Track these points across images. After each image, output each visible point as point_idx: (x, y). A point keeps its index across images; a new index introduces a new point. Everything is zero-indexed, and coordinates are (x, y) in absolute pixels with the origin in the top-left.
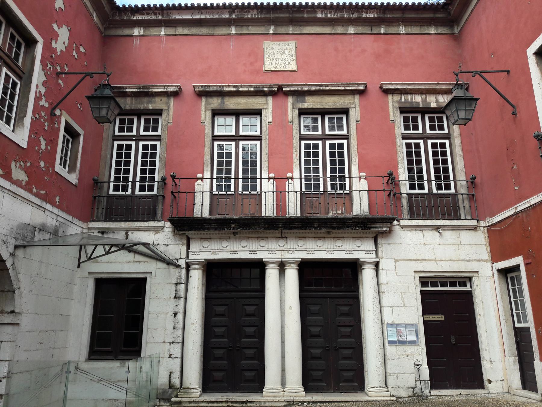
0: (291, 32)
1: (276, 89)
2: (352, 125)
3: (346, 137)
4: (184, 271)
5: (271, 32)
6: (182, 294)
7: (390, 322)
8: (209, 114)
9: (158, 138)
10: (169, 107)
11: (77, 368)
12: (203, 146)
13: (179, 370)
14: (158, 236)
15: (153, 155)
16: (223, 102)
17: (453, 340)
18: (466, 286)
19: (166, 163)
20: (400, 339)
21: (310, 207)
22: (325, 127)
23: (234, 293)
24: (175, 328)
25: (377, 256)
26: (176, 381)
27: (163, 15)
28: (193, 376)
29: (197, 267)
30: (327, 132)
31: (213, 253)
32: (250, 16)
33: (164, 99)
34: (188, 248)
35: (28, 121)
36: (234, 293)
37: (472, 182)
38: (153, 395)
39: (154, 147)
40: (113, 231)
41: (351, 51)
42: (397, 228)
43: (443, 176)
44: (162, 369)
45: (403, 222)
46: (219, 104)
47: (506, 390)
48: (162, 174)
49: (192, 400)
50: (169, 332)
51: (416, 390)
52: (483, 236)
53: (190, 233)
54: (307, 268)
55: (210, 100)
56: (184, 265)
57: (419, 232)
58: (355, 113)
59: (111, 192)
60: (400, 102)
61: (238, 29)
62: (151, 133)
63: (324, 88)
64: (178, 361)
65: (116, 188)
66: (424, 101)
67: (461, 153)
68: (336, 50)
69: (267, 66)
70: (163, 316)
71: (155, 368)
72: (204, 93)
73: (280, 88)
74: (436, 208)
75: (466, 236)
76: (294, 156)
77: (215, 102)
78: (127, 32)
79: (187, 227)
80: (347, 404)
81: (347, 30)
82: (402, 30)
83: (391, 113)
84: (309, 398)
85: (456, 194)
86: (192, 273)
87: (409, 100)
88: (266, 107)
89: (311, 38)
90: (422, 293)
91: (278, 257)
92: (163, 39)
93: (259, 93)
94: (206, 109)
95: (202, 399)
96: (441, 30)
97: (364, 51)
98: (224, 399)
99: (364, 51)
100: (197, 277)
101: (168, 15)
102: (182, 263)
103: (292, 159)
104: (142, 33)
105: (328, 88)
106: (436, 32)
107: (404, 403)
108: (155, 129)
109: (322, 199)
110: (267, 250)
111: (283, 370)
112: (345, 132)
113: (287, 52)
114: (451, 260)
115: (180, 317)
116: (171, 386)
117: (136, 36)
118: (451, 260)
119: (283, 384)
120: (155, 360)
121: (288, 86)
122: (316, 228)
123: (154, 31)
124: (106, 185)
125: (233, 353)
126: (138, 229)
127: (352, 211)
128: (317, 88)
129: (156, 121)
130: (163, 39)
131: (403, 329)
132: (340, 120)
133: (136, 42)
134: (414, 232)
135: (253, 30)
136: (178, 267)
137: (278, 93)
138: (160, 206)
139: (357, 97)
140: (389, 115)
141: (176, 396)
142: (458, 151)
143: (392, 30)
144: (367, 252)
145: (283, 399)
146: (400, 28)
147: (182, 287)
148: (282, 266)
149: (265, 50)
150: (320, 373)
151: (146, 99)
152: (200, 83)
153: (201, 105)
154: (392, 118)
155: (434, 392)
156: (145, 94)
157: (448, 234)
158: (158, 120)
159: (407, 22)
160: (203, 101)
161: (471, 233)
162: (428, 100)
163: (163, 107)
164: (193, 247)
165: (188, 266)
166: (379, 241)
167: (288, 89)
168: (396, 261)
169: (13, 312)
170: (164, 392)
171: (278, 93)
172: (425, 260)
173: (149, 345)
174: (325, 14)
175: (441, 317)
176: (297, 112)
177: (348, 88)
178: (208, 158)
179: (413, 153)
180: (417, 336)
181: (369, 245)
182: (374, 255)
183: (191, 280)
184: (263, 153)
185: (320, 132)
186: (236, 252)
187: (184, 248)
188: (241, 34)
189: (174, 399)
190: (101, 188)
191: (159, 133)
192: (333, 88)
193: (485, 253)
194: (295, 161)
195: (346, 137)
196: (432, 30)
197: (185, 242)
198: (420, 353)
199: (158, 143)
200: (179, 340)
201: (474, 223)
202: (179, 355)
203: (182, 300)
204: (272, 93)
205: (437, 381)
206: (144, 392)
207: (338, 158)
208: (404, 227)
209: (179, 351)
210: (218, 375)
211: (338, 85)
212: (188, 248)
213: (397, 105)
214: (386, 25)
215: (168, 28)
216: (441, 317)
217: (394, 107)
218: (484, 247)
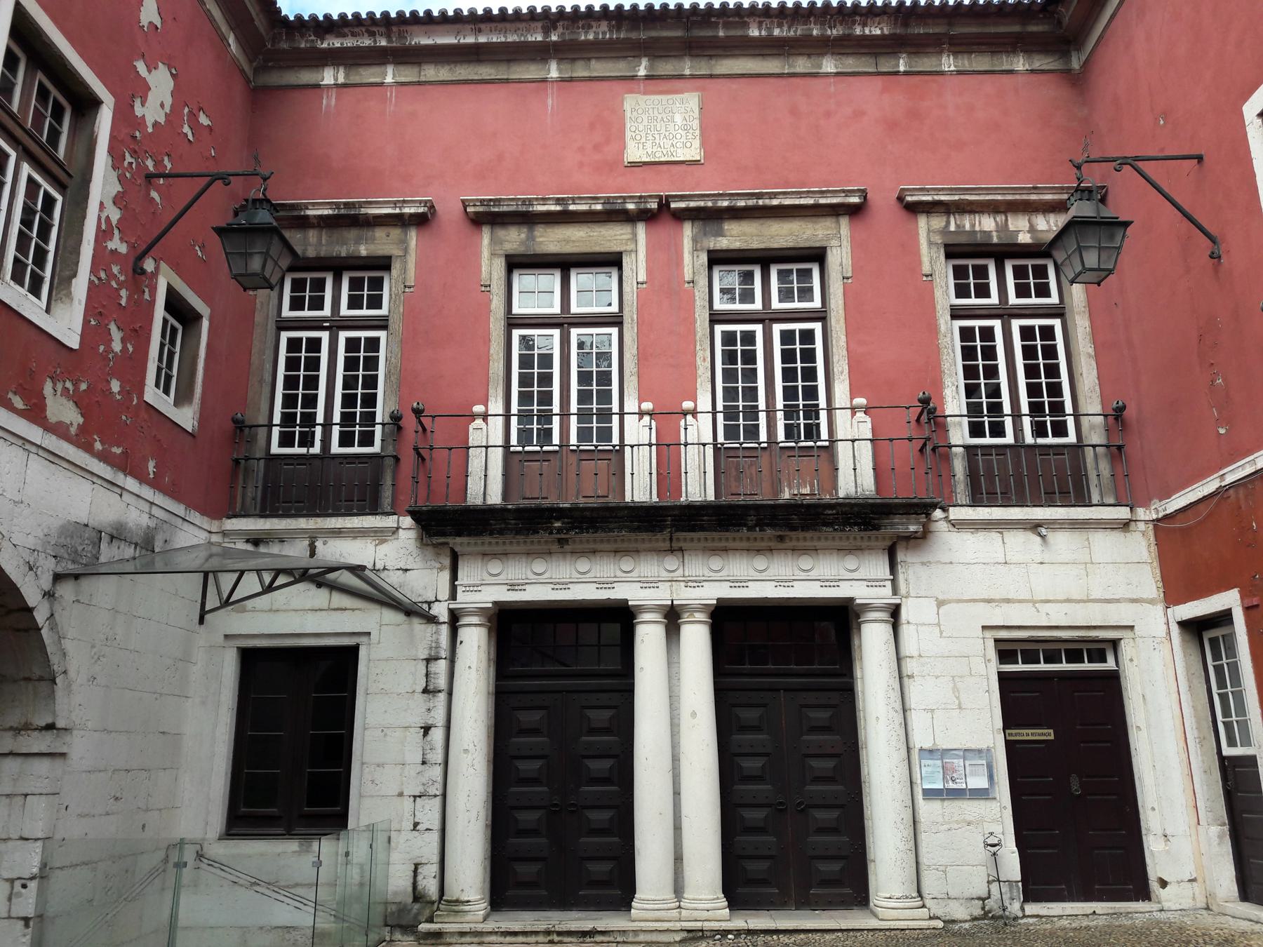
1: (654, 206)
3: (820, 316)
4: (445, 630)
5: (642, 72)
6: (442, 682)
8: (499, 266)
9: (382, 324)
10: (406, 250)
12: (487, 341)
13: (435, 858)
15: (372, 363)
16: (531, 238)
18: (1103, 660)
19: (402, 381)
20: (951, 785)
21: (738, 479)
22: (769, 291)
23: (560, 681)
24: (426, 762)
25: (895, 591)
26: (430, 886)
28: (469, 874)
29: (475, 620)
30: (776, 304)
31: (512, 587)
32: (591, 37)
34: (454, 576)
36: (560, 681)
37: (1116, 417)
38: (377, 919)
39: (373, 344)
41: (828, 114)
42: (942, 526)
43: (1047, 405)
44: (395, 856)
45: (955, 513)
46: (522, 243)
48: (393, 407)
49: (466, 927)
50: (412, 771)
52: (1144, 543)
53: (458, 542)
54: (729, 621)
55: (501, 233)
56: (444, 616)
57: (994, 535)
58: (840, 258)
59: (275, 449)
60: (945, 231)
62: (365, 312)
63: (767, 202)
64: (435, 837)
65: (286, 440)
67: (1091, 351)
68: (794, 111)
69: (635, 152)
71: (381, 856)
72: (488, 218)
73: (664, 204)
74: (1035, 479)
75: (1103, 543)
76: (699, 362)
77: (514, 239)
78: (306, 77)
79: (452, 527)
80: (828, 937)
82: (948, 63)
83: (925, 260)
84: (739, 923)
85: (1079, 447)
86: (464, 634)
87: (968, 227)
88: (631, 247)
91: (662, 595)
92: (391, 94)
93: (614, 215)
94: (493, 254)
95: (490, 926)
96: (1040, 62)
97: (858, 114)
98: (542, 926)
99: (858, 114)
100: (475, 644)
101: (402, 36)
102: (441, 611)
104: (341, 80)
105: (775, 202)
106: (1027, 67)
107: (961, 935)
108: (376, 302)
109: (764, 461)
110: (639, 581)
111: (678, 859)
112: (817, 303)
113: (678, 119)
114: (1068, 601)
115: (437, 735)
116: (418, 896)
118: (1068, 601)
120: (381, 837)
121: (682, 198)
122: (751, 529)
123: (368, 75)
124: (262, 432)
125: (560, 820)
126: (338, 533)
127: (835, 487)
128: (751, 202)
129: (377, 284)
130: (391, 94)
132: (805, 275)
133: (329, 101)
134: (981, 535)
135: (599, 68)
137: (660, 214)
138: (388, 480)
139: (844, 222)
140: (920, 263)
141: (430, 920)
142: (1084, 346)
143: (926, 63)
144: (872, 582)
145: (678, 925)
147: (441, 667)
148: (673, 617)
149: (628, 114)
150: (763, 865)
151: (352, 234)
152: (479, 194)
154: (926, 268)
155: (1031, 908)
156: (350, 220)
157: (1060, 540)
160: (486, 235)
161: (1116, 536)
162: (1011, 228)
163: (394, 251)
164: (467, 574)
165: (455, 618)
166: (900, 556)
167: (682, 205)
168: (940, 604)
169: (51, 727)
170: (402, 909)
171: (660, 214)
172: (1008, 601)
173: (367, 803)
175: (1048, 734)
176: (704, 258)
177: (822, 201)
178: (497, 367)
179: (977, 352)
180: (991, 777)
181: (878, 567)
183: (461, 650)
184: (627, 356)
185: (758, 305)
186: (565, 585)
187: (446, 576)
188: (571, 80)
189: (424, 927)
190: (252, 440)
191: (383, 311)
192: (787, 202)
193: (1149, 583)
194: (700, 372)
195: (820, 316)
197: (447, 562)
198: (998, 817)
199: (382, 334)
200: (436, 789)
201: (1123, 513)
202: (436, 825)
203: (442, 697)
204: (645, 216)
206: (356, 911)
208: (958, 525)
210: (526, 870)
212: (454, 576)
213: (938, 239)
214: (909, 54)
215: (402, 68)
216: (1048, 734)
217: (930, 243)
218: (1148, 568)
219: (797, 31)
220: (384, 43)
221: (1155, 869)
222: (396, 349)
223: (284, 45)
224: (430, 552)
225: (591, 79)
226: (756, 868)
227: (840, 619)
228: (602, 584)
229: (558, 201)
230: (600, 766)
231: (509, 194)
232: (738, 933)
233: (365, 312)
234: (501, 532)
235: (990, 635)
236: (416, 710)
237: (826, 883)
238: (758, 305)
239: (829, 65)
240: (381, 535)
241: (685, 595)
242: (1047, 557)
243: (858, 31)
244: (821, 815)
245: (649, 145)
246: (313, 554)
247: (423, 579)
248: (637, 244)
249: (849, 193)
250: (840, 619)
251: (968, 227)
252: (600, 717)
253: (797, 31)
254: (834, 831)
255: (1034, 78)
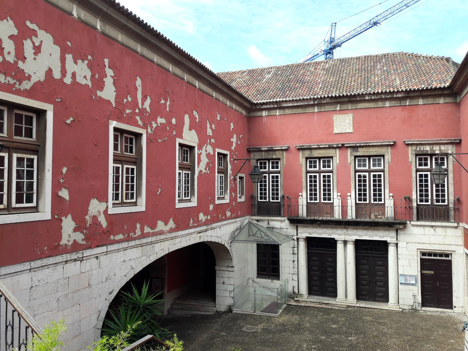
0: (350, 108)
2: (386, 164)
3: (383, 171)
4: (296, 242)
5: (338, 109)
6: (296, 252)
7: (402, 273)
8: (304, 159)
9: (279, 172)
10: (283, 157)
11: (253, 281)
13: (297, 286)
14: (283, 224)
15: (277, 181)
16: (311, 153)
17: (438, 284)
18: (449, 257)
19: (284, 187)
21: (361, 210)
22: (369, 165)
23: (321, 255)
24: (294, 266)
25: (397, 240)
26: (296, 291)
27: (277, 105)
28: (304, 289)
29: (302, 240)
30: (372, 168)
31: (310, 234)
33: (281, 152)
34: (297, 231)
35: (228, 191)
36: (321, 255)
37: (458, 201)
40: (262, 221)
41: (386, 118)
42: (410, 225)
43: (441, 194)
44: (289, 285)
45: (413, 223)
46: (309, 154)
47: (464, 312)
48: (282, 194)
49: (304, 300)
50: (292, 269)
51: (414, 307)
53: (298, 225)
54: (358, 244)
55: (304, 152)
56: (296, 239)
57: (422, 228)
58: (388, 157)
59: (259, 200)
60: (416, 150)
61: (319, 108)
62: (275, 170)
63: (369, 144)
64: (297, 282)
65: (261, 198)
66: (432, 149)
67: (453, 182)
68: (377, 118)
69: (336, 131)
70: (288, 261)
71: (286, 285)
72: (301, 149)
73: (343, 145)
75: (449, 231)
76: (352, 184)
77: (307, 153)
78: (259, 114)
79: (296, 222)
81: (385, 104)
82: (421, 102)
83: (410, 158)
84: (358, 305)
86: (300, 243)
87: (422, 149)
88: (335, 155)
89: (361, 111)
90: (421, 259)
91: (343, 238)
93: (330, 147)
94: (303, 157)
95: (308, 300)
96: (448, 100)
97: (395, 118)
98: (318, 301)
99: (395, 118)
100: (302, 245)
101: (280, 104)
102: (295, 238)
103: (350, 184)
104: (267, 114)
105: (371, 144)
106: (444, 102)
107: (406, 313)
108: (277, 167)
109: (368, 206)
110: (338, 235)
111: (346, 290)
112: (382, 168)
113: (347, 121)
114: (439, 244)
115: (296, 262)
116: (294, 293)
117: (264, 116)
118: (439, 244)
119: (346, 296)
121: (347, 144)
122: (362, 226)
123: (273, 113)
124: (256, 198)
126: (273, 220)
128: (365, 144)
129: (277, 163)
130: (279, 118)
131: (409, 278)
132: (379, 160)
133: (265, 120)
134: (419, 228)
135: (328, 108)
136: (294, 240)
137: (342, 147)
139: (389, 148)
140: (408, 159)
141: (297, 297)
142: (451, 181)
143: (414, 102)
145: (345, 304)
146: (420, 100)
147: (296, 249)
148: (345, 242)
149: (334, 120)
150: (366, 292)
151: (271, 153)
153: (299, 155)
154: (410, 160)
155: (423, 309)
158: (278, 162)
159: (424, 97)
161: (454, 230)
162: (434, 149)
163: (281, 157)
164: (300, 230)
165: (298, 239)
166: (399, 232)
167: (347, 145)
168: (407, 243)
169: (232, 267)
170: (291, 295)
171: (342, 147)
172: (424, 243)
173: (283, 274)
174: (371, 97)
175: (433, 272)
176: (353, 158)
178: (304, 184)
179: (423, 180)
180: (416, 281)
181: (393, 234)
182: (395, 239)
187: (295, 230)
188: (320, 112)
189: (296, 299)
190: (255, 199)
191: (279, 169)
192: (374, 144)
193: (461, 241)
194: (352, 186)
195: (383, 171)
196: (442, 101)
197: (295, 227)
198: (417, 290)
199: (279, 175)
200: (296, 273)
201: (456, 225)
202: (297, 280)
203: (296, 255)
204: (339, 148)
205: (424, 304)
206: (283, 294)
207: (377, 181)
209: (297, 278)
211: (377, 142)
212: (297, 231)
213: (414, 153)
214: (410, 99)
216: (433, 272)
217: (412, 154)
218: (461, 238)
219: (379, 97)
220: (276, 106)
221: (454, 304)
222: (282, 180)
223: (254, 108)
224: (292, 225)
225: (325, 111)
226: (364, 292)
227: (385, 245)
228: (329, 234)
229: (317, 145)
230: (331, 269)
231: (306, 145)
232: (358, 307)
233: (275, 170)
234: (306, 224)
235: (418, 250)
236: (291, 257)
237: (379, 297)
238: (367, 168)
239: (387, 104)
240: (282, 221)
241: (348, 238)
242: (435, 234)
243: (395, 96)
244: (379, 283)
245: (340, 128)
246: (269, 224)
247: (291, 231)
248: (337, 155)
249: (390, 142)
250: (385, 245)
251: (422, 149)
252: (330, 259)
253: (379, 97)
254: (382, 287)
255: (445, 105)
